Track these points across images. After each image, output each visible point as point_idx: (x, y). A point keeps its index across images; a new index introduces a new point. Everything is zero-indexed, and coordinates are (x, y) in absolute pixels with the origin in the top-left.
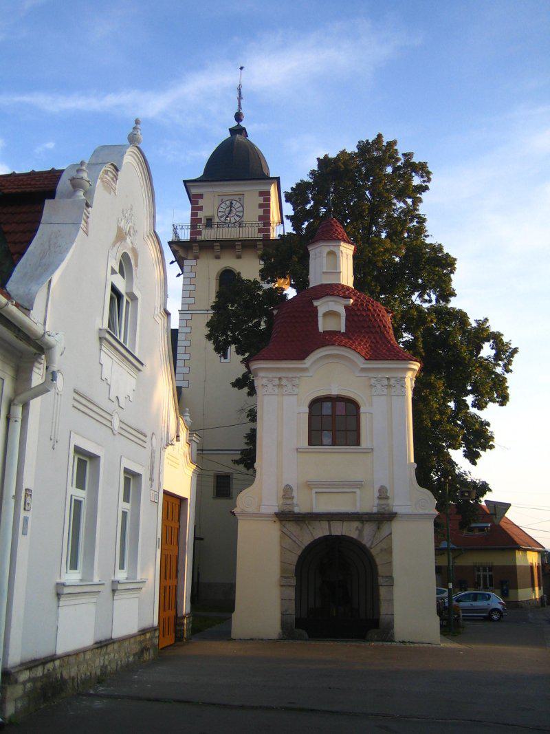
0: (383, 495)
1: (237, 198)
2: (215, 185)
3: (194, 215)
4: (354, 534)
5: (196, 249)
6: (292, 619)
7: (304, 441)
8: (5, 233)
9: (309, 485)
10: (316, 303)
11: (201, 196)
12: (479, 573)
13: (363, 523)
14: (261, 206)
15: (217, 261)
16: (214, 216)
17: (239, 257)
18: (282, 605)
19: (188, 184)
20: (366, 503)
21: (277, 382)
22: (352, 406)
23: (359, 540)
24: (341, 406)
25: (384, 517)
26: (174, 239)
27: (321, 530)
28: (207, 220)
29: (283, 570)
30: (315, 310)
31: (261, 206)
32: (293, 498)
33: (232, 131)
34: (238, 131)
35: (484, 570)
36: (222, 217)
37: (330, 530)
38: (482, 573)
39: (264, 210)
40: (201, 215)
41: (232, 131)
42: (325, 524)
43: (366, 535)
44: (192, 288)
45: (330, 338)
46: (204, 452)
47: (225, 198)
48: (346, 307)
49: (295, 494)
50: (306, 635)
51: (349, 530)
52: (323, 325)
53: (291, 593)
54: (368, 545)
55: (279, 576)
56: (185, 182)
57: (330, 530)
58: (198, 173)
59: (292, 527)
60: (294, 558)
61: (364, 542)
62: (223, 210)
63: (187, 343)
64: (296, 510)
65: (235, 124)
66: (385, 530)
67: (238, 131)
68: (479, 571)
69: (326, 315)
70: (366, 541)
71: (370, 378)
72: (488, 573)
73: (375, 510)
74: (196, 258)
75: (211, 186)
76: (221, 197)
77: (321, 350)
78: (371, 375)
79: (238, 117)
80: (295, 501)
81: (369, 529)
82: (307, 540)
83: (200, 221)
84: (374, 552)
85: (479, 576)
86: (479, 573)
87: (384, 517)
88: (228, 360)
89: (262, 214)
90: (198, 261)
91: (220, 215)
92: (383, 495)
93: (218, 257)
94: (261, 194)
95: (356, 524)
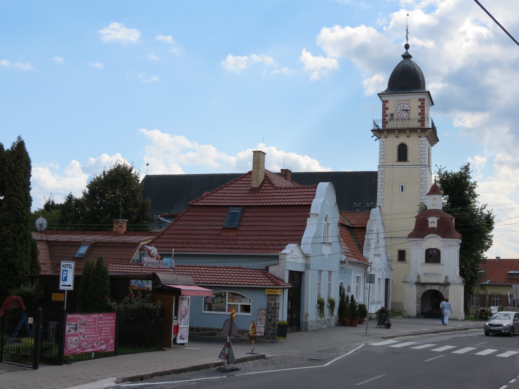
0: (447, 278)
1: (406, 102)
2: (395, 96)
3: (384, 112)
4: (438, 289)
5: (385, 132)
6: (420, 312)
7: (424, 262)
8: (358, 238)
9: (425, 274)
10: (428, 219)
11: (387, 102)
12: (494, 299)
13: (440, 286)
14: (420, 107)
15: (397, 138)
16: (394, 113)
17: (408, 137)
18: (417, 308)
19: (380, 95)
20: (442, 280)
21: (415, 244)
22: (438, 252)
23: (439, 291)
24: (435, 251)
25: (447, 284)
26: (376, 128)
27: (428, 288)
28: (391, 115)
29: (417, 299)
30: (428, 221)
31: (420, 107)
32: (420, 278)
33: (403, 56)
34: (406, 57)
35: (497, 297)
36: (399, 113)
37: (431, 288)
38: (495, 299)
39: (421, 110)
40: (387, 112)
41: (403, 56)
42: (429, 286)
43: (441, 289)
44: (384, 147)
45: (433, 231)
46: (393, 167)
47: (400, 102)
48: (437, 220)
49: (421, 277)
50: (424, 317)
51: (436, 288)
52: (431, 225)
53: (419, 305)
54: (442, 292)
55: (416, 300)
56: (378, 94)
57: (431, 288)
58: (384, 87)
59: (419, 287)
60: (420, 296)
61: (440, 292)
62: (400, 108)
63: (382, 183)
64: (421, 282)
65: (405, 51)
66: (447, 288)
67: (406, 57)
68: (494, 297)
69: (432, 222)
70: (441, 291)
71: (444, 243)
72: (498, 299)
73: (444, 282)
74: (386, 137)
75: (393, 96)
76: (398, 102)
77: (428, 235)
78: (444, 242)
79: (407, 47)
80: (421, 279)
81: (442, 288)
82: (424, 291)
83: (387, 115)
84: (443, 294)
85: (494, 301)
86: (494, 299)
87: (447, 284)
88: (403, 192)
89: (420, 105)
90: (387, 139)
91: (398, 112)
92: (447, 278)
93: (397, 137)
94: (420, 100)
95: (438, 286)
